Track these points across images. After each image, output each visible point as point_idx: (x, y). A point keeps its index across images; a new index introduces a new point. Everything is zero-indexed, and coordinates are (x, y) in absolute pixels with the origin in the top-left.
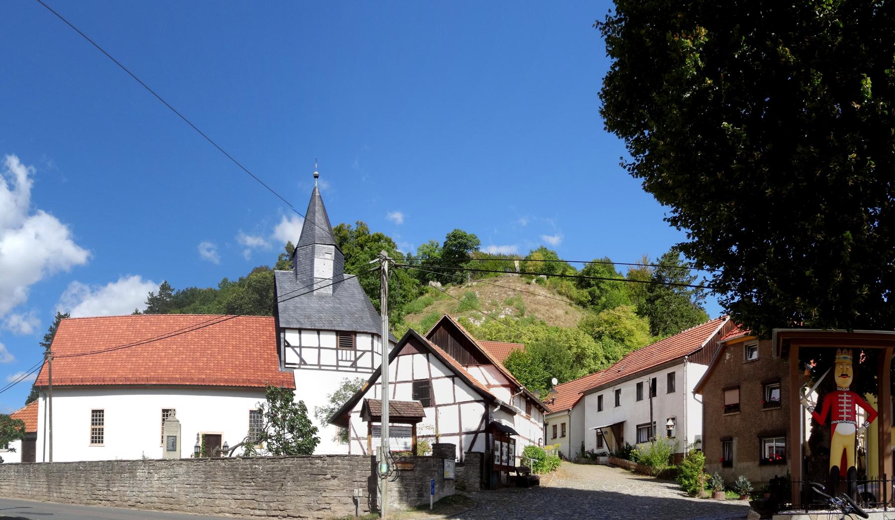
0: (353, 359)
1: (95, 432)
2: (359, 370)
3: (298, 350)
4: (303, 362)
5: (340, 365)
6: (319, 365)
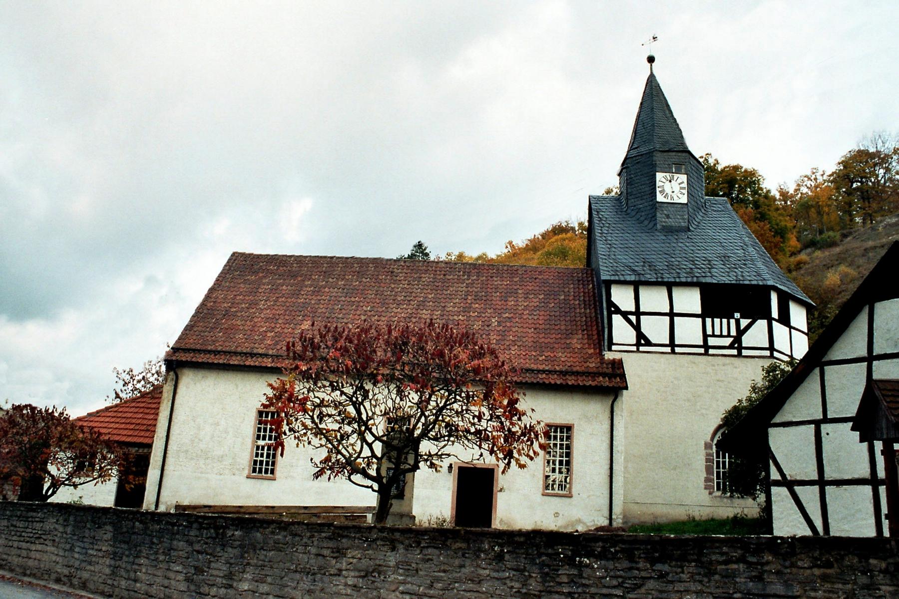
0: (733, 332)
1: (260, 452)
2: (745, 352)
3: (633, 318)
4: (642, 340)
5: (710, 343)
6: (672, 344)
